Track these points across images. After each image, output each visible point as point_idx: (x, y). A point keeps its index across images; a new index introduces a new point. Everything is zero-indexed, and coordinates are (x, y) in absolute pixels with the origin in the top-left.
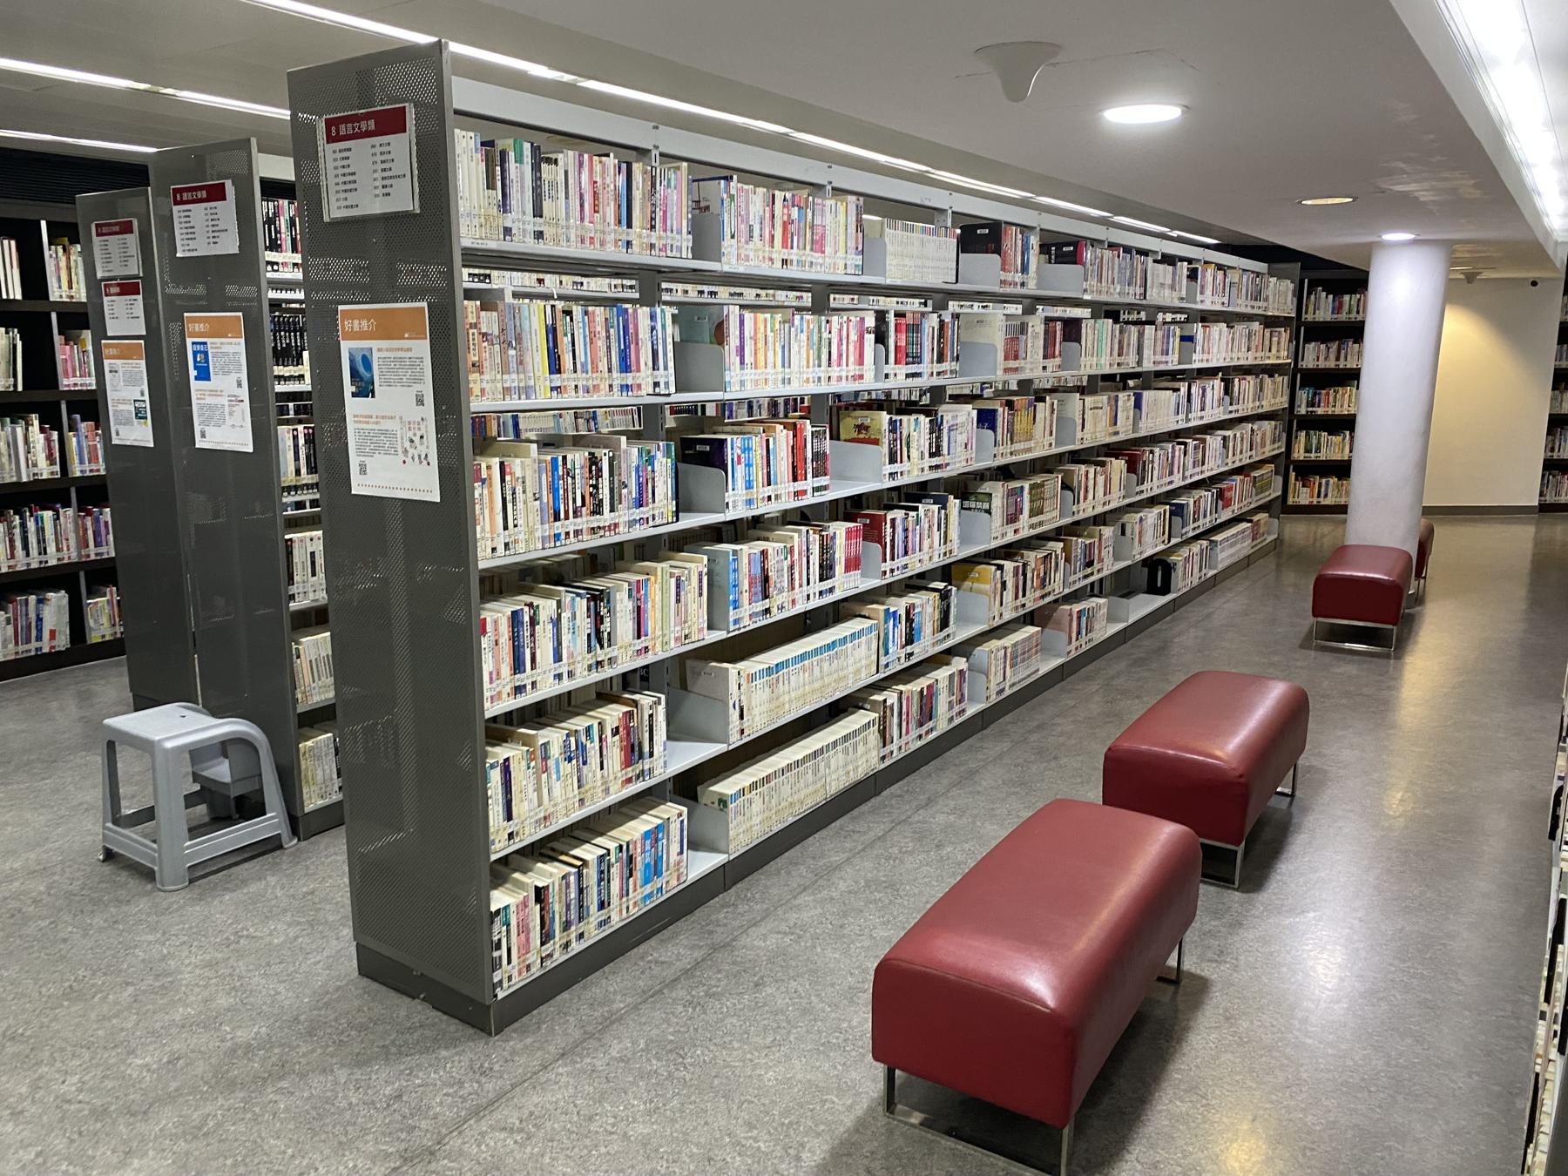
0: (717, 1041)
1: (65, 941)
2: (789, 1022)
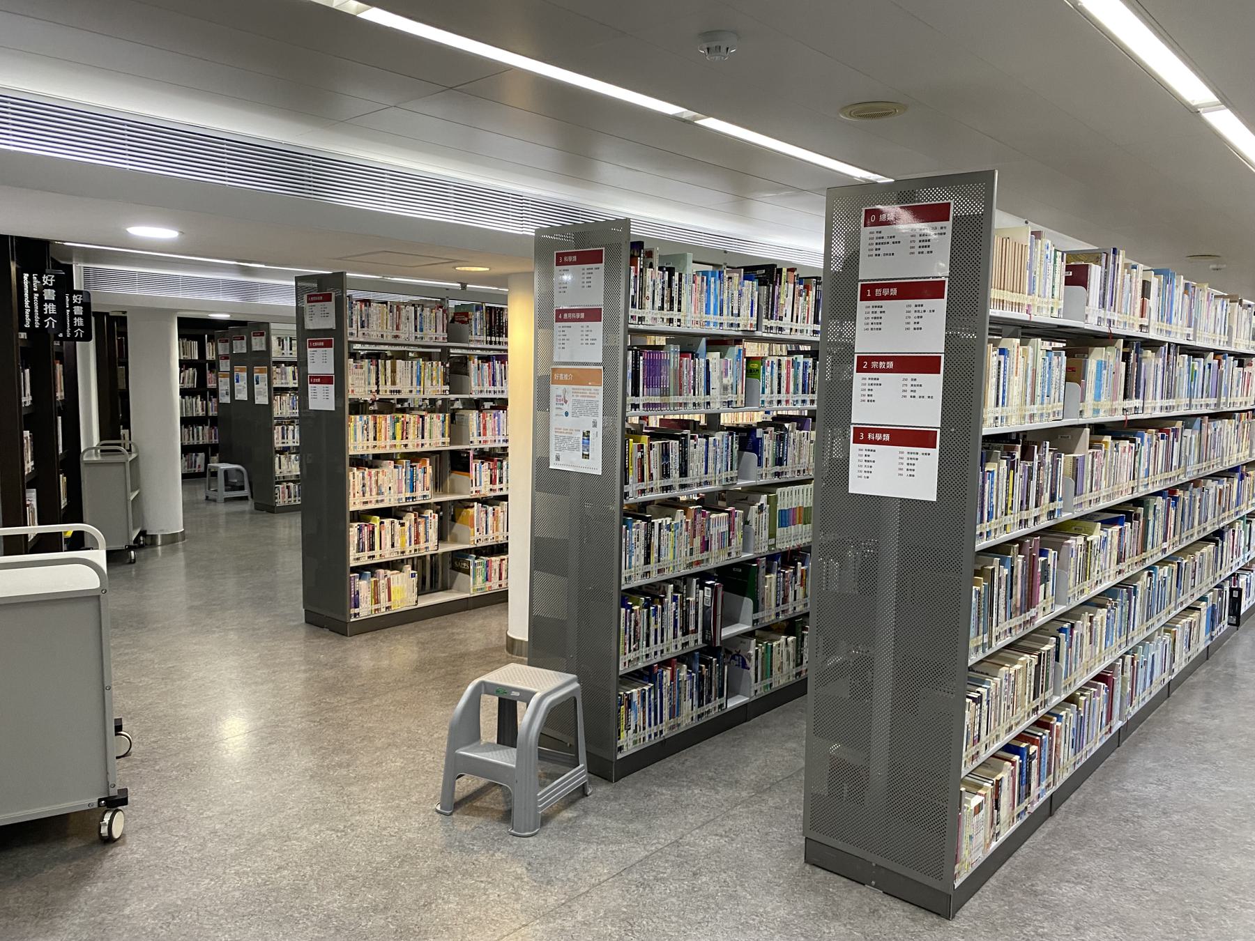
0: (660, 915)
1: (193, 800)
2: (717, 905)
